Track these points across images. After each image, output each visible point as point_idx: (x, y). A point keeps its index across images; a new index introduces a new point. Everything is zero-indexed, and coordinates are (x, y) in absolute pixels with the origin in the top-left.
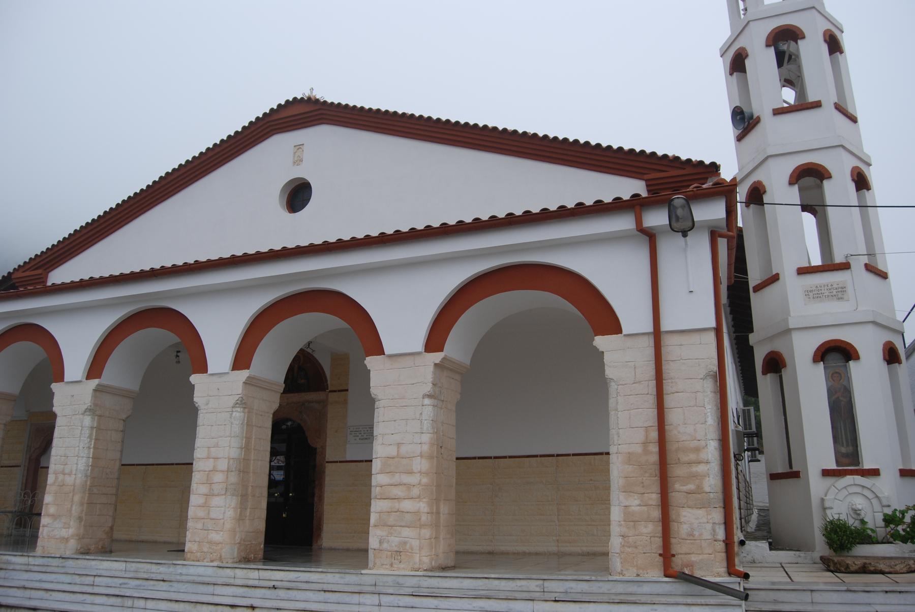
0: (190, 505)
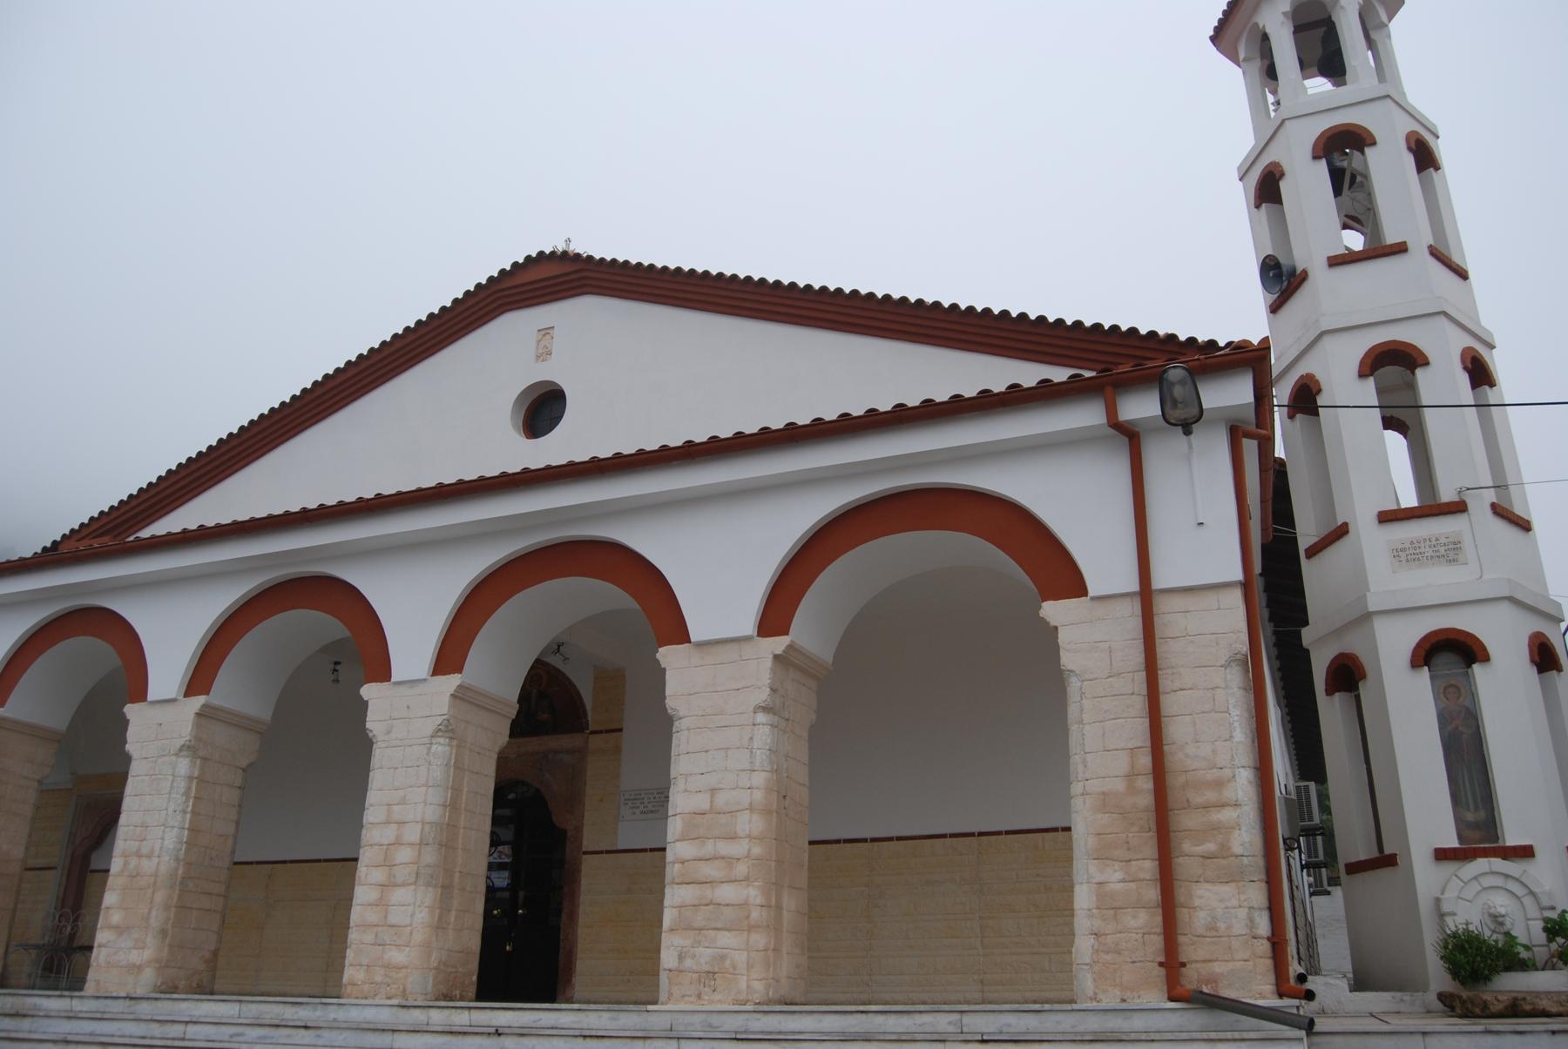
0: (354, 903)
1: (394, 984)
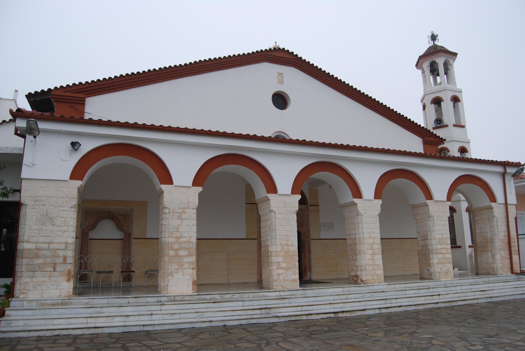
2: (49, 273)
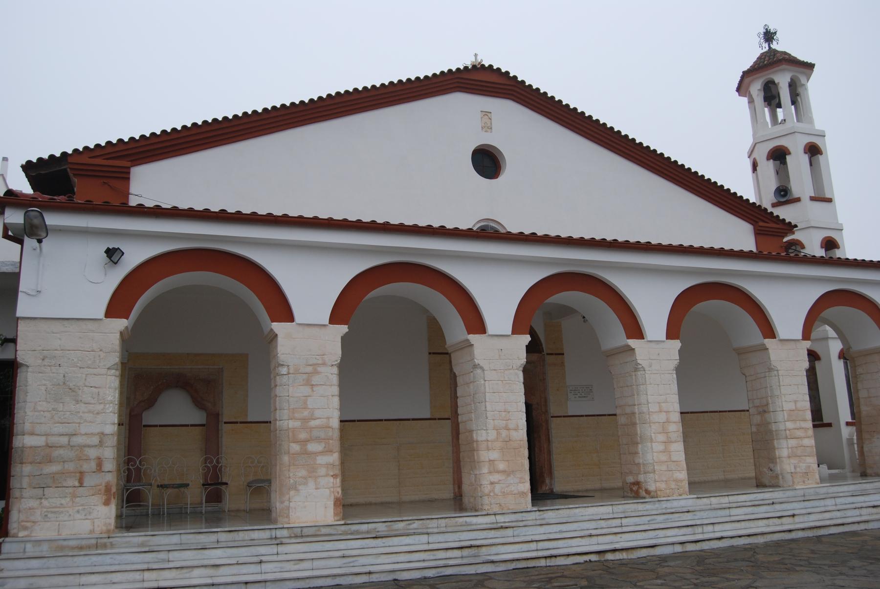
1: (681, 488)
2: (71, 490)
